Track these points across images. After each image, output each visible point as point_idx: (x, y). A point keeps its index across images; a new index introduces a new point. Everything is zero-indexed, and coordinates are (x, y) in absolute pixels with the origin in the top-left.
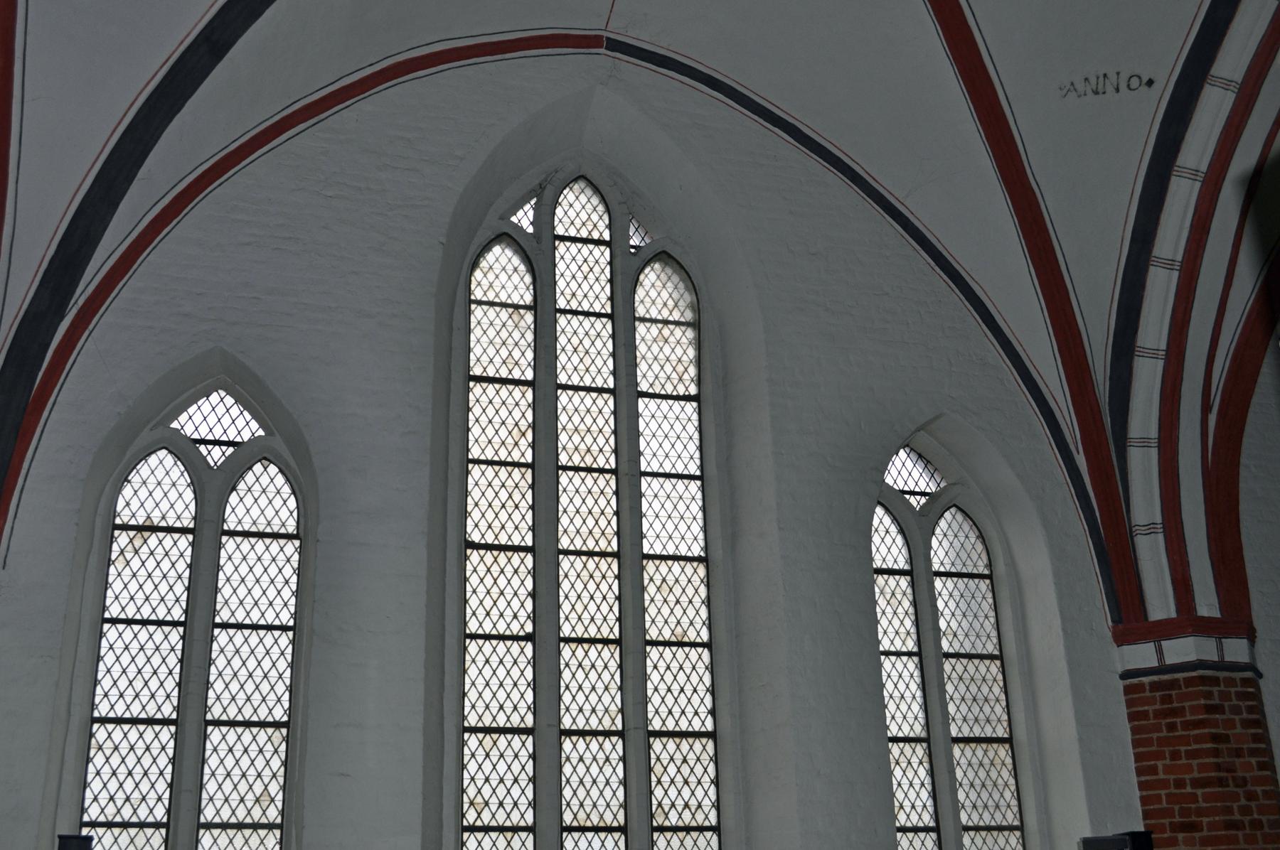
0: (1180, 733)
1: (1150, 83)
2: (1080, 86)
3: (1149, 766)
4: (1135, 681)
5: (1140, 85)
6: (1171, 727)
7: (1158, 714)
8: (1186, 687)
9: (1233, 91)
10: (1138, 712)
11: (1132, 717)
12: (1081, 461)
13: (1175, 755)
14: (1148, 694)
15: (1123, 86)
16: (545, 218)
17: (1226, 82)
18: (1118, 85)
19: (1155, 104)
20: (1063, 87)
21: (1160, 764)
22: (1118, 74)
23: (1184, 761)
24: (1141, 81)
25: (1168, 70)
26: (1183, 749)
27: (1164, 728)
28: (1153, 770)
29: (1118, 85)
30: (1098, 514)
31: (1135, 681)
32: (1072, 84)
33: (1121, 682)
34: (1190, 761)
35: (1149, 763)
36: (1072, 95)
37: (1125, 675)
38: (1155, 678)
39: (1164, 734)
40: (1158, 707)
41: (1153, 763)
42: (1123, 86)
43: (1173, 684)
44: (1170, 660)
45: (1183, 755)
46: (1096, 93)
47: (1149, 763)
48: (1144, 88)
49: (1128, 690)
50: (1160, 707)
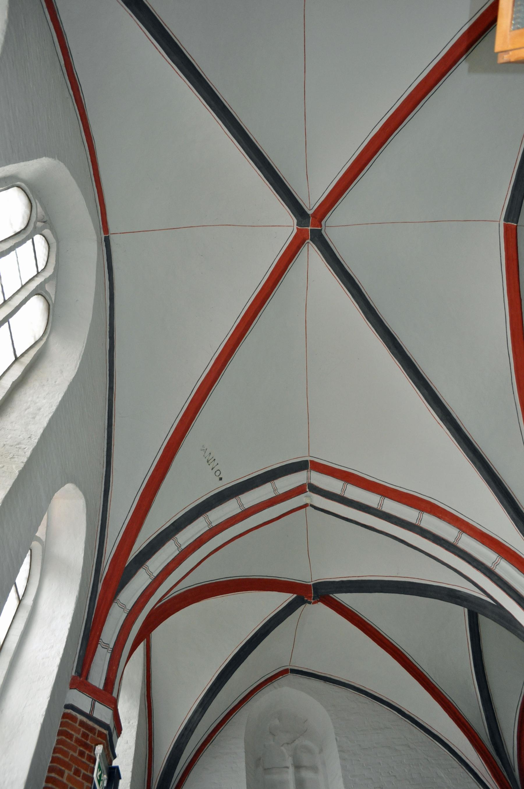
0: (84, 760)
3: (60, 770)
4: (74, 713)
5: (218, 476)
6: (82, 754)
7: (77, 741)
8: (98, 736)
9: (454, 542)
10: (69, 732)
11: (60, 733)
13: (77, 772)
14: (77, 725)
15: (215, 470)
17: (458, 540)
18: (214, 468)
20: (204, 446)
21: (67, 772)
22: (218, 464)
23: (80, 779)
24: (219, 475)
25: (230, 480)
26: (83, 771)
27: (78, 752)
28: (61, 773)
29: (214, 468)
30: (93, 616)
31: (74, 713)
32: (206, 449)
33: (64, 709)
34: (84, 782)
35: (61, 767)
36: (203, 452)
37: (69, 706)
38: (85, 719)
39: (76, 755)
40: (79, 736)
41: (63, 768)
42: (215, 470)
43: (92, 730)
44: (96, 715)
45: (81, 775)
46: (208, 462)
47: (61, 767)
48: (218, 478)
49: (65, 716)
50: (81, 738)
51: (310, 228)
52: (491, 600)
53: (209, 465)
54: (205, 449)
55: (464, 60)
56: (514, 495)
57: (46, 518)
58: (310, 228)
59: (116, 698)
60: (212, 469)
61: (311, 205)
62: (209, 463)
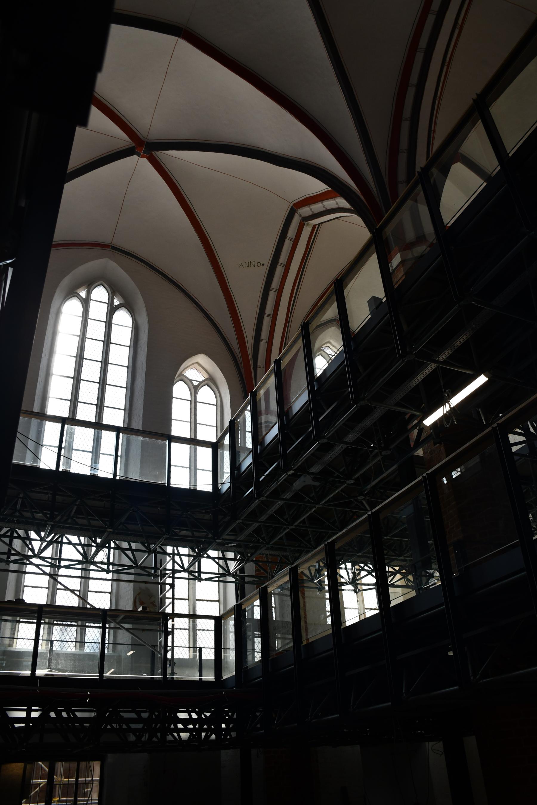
1: (263, 265)
2: (244, 264)
12: (243, 371)
15: (256, 265)
16: (89, 294)
19: (263, 271)
22: (254, 262)
24: (261, 264)
25: (267, 260)
32: (241, 264)
36: (241, 267)
42: (256, 265)
46: (248, 267)
48: (261, 266)
51: (142, 153)
52: (73, 562)
53: (250, 267)
54: (240, 264)
55: (402, 596)
56: (97, 157)
57: (312, 571)
58: (142, 153)
59: (323, 381)
60: (254, 266)
61: (208, 646)
62: (249, 266)
